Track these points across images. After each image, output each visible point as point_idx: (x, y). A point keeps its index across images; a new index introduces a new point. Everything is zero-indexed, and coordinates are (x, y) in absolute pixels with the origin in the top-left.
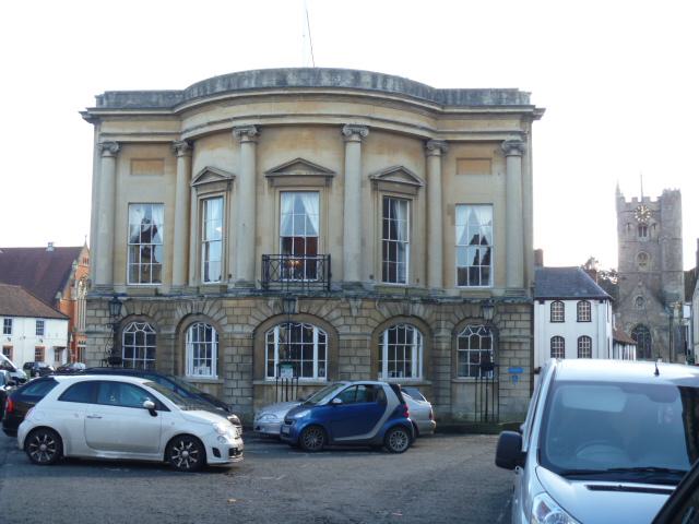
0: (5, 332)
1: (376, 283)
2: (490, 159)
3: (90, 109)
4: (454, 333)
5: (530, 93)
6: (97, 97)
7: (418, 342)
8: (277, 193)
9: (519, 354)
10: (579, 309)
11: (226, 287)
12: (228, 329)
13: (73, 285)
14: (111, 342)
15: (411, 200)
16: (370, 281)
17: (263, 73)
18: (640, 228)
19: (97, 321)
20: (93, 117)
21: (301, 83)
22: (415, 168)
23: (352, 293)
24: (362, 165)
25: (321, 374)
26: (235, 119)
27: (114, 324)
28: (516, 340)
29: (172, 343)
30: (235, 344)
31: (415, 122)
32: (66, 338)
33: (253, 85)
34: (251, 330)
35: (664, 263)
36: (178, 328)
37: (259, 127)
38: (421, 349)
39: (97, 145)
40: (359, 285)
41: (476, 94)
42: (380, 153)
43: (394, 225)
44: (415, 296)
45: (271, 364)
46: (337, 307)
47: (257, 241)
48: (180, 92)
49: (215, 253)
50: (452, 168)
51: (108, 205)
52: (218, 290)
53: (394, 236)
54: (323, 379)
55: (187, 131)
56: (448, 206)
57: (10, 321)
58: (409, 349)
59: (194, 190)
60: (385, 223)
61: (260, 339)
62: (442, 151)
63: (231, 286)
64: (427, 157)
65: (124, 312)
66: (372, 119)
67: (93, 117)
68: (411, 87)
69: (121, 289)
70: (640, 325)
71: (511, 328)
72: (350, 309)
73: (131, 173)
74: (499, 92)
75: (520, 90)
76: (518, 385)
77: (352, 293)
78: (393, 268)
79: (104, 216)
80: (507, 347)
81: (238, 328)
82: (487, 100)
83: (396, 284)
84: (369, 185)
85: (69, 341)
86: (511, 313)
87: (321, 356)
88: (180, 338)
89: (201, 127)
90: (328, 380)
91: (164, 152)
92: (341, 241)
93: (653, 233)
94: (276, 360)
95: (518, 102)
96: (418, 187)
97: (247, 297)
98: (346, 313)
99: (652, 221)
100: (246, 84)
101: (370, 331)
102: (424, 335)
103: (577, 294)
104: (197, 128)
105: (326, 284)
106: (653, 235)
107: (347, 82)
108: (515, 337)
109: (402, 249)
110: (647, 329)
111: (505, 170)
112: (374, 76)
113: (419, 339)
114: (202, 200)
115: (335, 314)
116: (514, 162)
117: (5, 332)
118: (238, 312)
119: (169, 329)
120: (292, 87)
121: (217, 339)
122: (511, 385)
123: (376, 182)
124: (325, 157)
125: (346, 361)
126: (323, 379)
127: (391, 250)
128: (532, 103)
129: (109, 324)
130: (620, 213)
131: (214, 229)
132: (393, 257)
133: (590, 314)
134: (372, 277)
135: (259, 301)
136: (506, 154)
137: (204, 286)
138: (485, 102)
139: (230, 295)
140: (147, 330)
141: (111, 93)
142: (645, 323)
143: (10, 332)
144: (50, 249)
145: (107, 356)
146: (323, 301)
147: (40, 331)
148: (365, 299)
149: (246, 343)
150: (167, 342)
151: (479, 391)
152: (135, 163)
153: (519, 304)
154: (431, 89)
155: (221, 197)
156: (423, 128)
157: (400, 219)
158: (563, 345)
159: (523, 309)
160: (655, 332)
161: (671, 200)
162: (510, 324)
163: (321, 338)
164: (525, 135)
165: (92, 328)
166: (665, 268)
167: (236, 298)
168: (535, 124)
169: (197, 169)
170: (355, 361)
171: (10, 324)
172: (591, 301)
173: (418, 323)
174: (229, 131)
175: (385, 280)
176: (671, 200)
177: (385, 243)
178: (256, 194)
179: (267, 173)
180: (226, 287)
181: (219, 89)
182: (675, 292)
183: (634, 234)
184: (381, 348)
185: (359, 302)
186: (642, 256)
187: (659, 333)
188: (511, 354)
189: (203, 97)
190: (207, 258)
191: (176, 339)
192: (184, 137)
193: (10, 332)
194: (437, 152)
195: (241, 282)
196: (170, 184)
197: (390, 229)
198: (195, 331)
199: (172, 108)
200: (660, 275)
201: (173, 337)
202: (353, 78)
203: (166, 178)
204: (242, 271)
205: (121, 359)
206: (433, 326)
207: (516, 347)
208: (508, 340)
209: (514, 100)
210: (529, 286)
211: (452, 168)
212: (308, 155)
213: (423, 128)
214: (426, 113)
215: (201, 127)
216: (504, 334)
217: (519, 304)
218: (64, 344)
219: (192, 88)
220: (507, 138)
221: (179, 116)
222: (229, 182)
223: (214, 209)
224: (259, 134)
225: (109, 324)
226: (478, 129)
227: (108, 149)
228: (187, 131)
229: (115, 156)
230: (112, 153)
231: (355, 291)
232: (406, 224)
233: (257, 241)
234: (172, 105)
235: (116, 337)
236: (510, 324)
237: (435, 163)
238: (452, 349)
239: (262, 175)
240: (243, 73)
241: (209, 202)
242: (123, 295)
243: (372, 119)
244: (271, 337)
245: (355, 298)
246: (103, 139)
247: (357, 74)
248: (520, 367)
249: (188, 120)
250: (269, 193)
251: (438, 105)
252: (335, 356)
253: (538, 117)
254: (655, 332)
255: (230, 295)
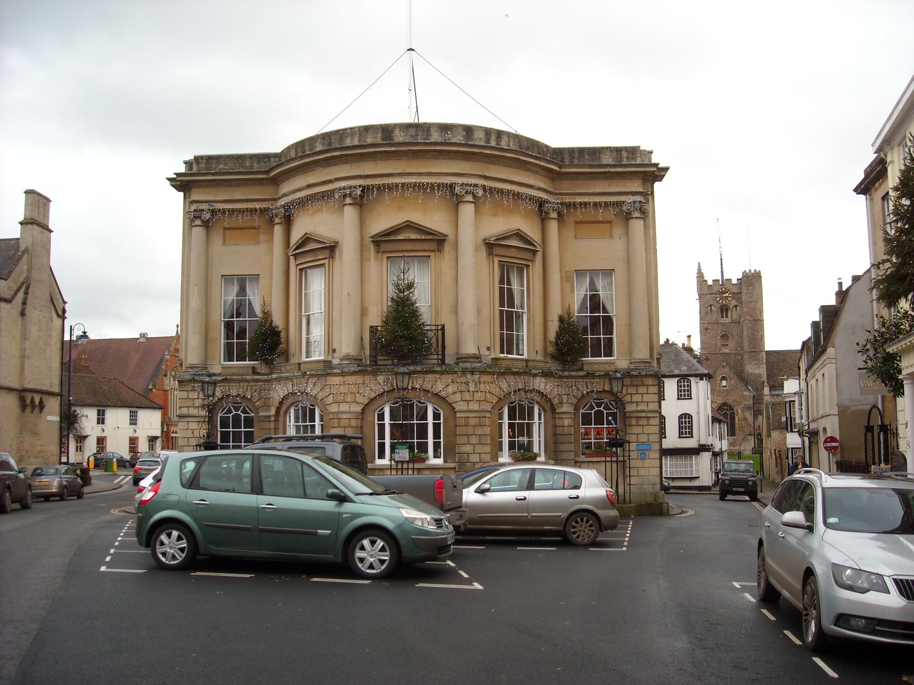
0: (98, 423)
1: (493, 356)
2: (610, 222)
3: (178, 175)
4: (576, 408)
5: (651, 152)
6: (186, 163)
7: (540, 419)
8: (385, 259)
9: (648, 430)
10: (679, 386)
11: (330, 362)
12: (334, 408)
13: (166, 376)
14: (205, 426)
15: (528, 266)
16: (487, 353)
17: (367, 129)
18: (722, 310)
19: (190, 403)
20: (181, 183)
21: (409, 140)
22: (532, 231)
23: (468, 365)
24: (477, 227)
25: (436, 456)
26: (337, 180)
27: (209, 406)
28: (643, 415)
29: (272, 425)
30: (342, 424)
31: (531, 182)
32: (160, 427)
33: (356, 143)
34: (358, 409)
35: (746, 344)
36: (278, 409)
37: (365, 190)
38: (542, 426)
39: (186, 213)
40: (477, 358)
41: (595, 152)
42: (495, 215)
43: (510, 291)
44: (535, 368)
45: (382, 446)
46: (453, 382)
47: (364, 312)
48: (276, 155)
49: (318, 332)
50: (570, 231)
51: (198, 276)
52: (321, 366)
53: (511, 304)
54: (439, 461)
55: (285, 195)
56: (567, 272)
57: (104, 411)
58: (530, 426)
59: (292, 258)
60: (501, 290)
61: (369, 418)
62: (559, 214)
63: (336, 362)
64: (543, 220)
65: (218, 394)
66: (485, 178)
67: (181, 183)
68: (526, 144)
69: (216, 369)
70: (725, 404)
71: (638, 400)
72: (467, 383)
73: (224, 243)
74: (618, 150)
75: (642, 148)
76: (647, 463)
77: (468, 365)
78: (510, 339)
79: (196, 289)
80: (634, 422)
81: (344, 407)
82: (607, 159)
83: (376, 422)
84: (483, 252)
85: (162, 431)
86: (637, 386)
87: (437, 435)
88: (281, 419)
89: (299, 190)
90: (445, 462)
91: (257, 221)
92: (455, 311)
93: (734, 314)
94: (387, 441)
95: (639, 161)
96: (535, 252)
97: (354, 373)
98: (463, 388)
99: (734, 303)
100: (348, 142)
101: (488, 407)
102: (545, 411)
103: (677, 372)
104: (294, 192)
105: (440, 357)
106: (734, 316)
107: (459, 138)
108: (643, 411)
109: (519, 316)
110: (731, 408)
111: (627, 233)
112: (488, 132)
113: (540, 415)
114: (301, 270)
115: (450, 389)
116: (637, 225)
117: (98, 423)
118: (343, 389)
119: (269, 411)
120: (399, 144)
121: (322, 420)
122: (639, 463)
123: (491, 246)
124: (434, 219)
125: (464, 440)
126: (439, 461)
127: (509, 321)
128: (654, 161)
129: (203, 407)
130: (701, 296)
131: (317, 305)
132: (510, 328)
133: (690, 391)
134: (488, 349)
135: (367, 377)
136: (628, 217)
137: (306, 362)
138: (605, 162)
139: (335, 371)
140: (244, 412)
141: (202, 157)
142: (730, 402)
143: (103, 423)
144: (142, 340)
145: (202, 441)
146: (438, 376)
147: (133, 421)
148: (483, 372)
149: (354, 423)
150: (266, 425)
151: (609, 470)
152: (228, 232)
153: (646, 376)
154: (547, 147)
155: (323, 265)
156: (539, 189)
157: (515, 287)
158: (691, 422)
159: (650, 381)
160: (740, 411)
161: (752, 280)
162: (637, 398)
163: (436, 416)
164: (649, 195)
165: (185, 411)
166: (746, 348)
167: (343, 374)
168: (657, 185)
169: (296, 235)
170: (474, 440)
171: (104, 415)
172: (692, 379)
173: (543, 402)
174: (332, 192)
175: (502, 352)
176: (752, 280)
177: (501, 312)
178: (362, 260)
179: (371, 237)
180: (330, 362)
181: (319, 147)
182: (757, 372)
183: (715, 315)
184: (501, 425)
185: (477, 377)
186: (724, 337)
187: (742, 411)
188: (637, 430)
189: (302, 157)
190: (308, 333)
191: (277, 421)
192: (282, 202)
193: (103, 423)
194: (554, 215)
195: (347, 357)
196: (262, 257)
197: (506, 297)
198: (296, 411)
199: (267, 172)
200: (742, 356)
201: (273, 419)
202: (465, 134)
203: (263, 247)
204: (347, 345)
205: (216, 443)
206: (556, 401)
207: (644, 422)
208: (635, 415)
209: (635, 159)
210: (655, 356)
211: (570, 231)
212: (418, 217)
213: (539, 189)
214: (542, 172)
215: (299, 190)
216: (630, 408)
217: (646, 376)
218: (158, 433)
219: (288, 149)
220: (630, 199)
221: (275, 181)
222: (332, 249)
223: (317, 284)
224: (363, 199)
225: (203, 407)
226: (598, 191)
227: (199, 217)
228: (285, 195)
229: (206, 225)
230: (203, 221)
231: (469, 366)
232: (522, 291)
233: (364, 312)
234: (263, 171)
235: (211, 420)
236: (637, 398)
237: (553, 226)
238: (575, 426)
239: (368, 240)
240: (345, 130)
241: (309, 271)
242: (219, 375)
243: (485, 178)
244: (381, 417)
245: (472, 372)
246: (194, 207)
247: (469, 130)
248: (648, 443)
249: (286, 183)
250: (376, 259)
251: (555, 164)
252: (452, 435)
253: (660, 178)
254: (740, 411)
255: (335, 371)
